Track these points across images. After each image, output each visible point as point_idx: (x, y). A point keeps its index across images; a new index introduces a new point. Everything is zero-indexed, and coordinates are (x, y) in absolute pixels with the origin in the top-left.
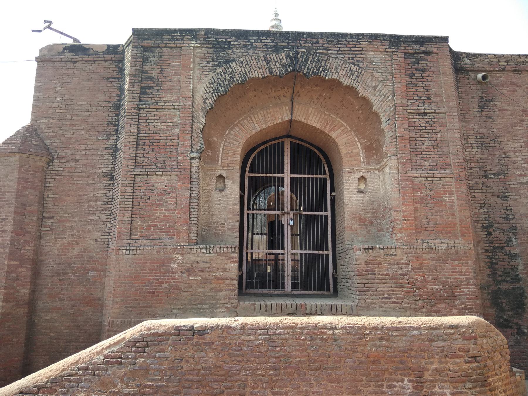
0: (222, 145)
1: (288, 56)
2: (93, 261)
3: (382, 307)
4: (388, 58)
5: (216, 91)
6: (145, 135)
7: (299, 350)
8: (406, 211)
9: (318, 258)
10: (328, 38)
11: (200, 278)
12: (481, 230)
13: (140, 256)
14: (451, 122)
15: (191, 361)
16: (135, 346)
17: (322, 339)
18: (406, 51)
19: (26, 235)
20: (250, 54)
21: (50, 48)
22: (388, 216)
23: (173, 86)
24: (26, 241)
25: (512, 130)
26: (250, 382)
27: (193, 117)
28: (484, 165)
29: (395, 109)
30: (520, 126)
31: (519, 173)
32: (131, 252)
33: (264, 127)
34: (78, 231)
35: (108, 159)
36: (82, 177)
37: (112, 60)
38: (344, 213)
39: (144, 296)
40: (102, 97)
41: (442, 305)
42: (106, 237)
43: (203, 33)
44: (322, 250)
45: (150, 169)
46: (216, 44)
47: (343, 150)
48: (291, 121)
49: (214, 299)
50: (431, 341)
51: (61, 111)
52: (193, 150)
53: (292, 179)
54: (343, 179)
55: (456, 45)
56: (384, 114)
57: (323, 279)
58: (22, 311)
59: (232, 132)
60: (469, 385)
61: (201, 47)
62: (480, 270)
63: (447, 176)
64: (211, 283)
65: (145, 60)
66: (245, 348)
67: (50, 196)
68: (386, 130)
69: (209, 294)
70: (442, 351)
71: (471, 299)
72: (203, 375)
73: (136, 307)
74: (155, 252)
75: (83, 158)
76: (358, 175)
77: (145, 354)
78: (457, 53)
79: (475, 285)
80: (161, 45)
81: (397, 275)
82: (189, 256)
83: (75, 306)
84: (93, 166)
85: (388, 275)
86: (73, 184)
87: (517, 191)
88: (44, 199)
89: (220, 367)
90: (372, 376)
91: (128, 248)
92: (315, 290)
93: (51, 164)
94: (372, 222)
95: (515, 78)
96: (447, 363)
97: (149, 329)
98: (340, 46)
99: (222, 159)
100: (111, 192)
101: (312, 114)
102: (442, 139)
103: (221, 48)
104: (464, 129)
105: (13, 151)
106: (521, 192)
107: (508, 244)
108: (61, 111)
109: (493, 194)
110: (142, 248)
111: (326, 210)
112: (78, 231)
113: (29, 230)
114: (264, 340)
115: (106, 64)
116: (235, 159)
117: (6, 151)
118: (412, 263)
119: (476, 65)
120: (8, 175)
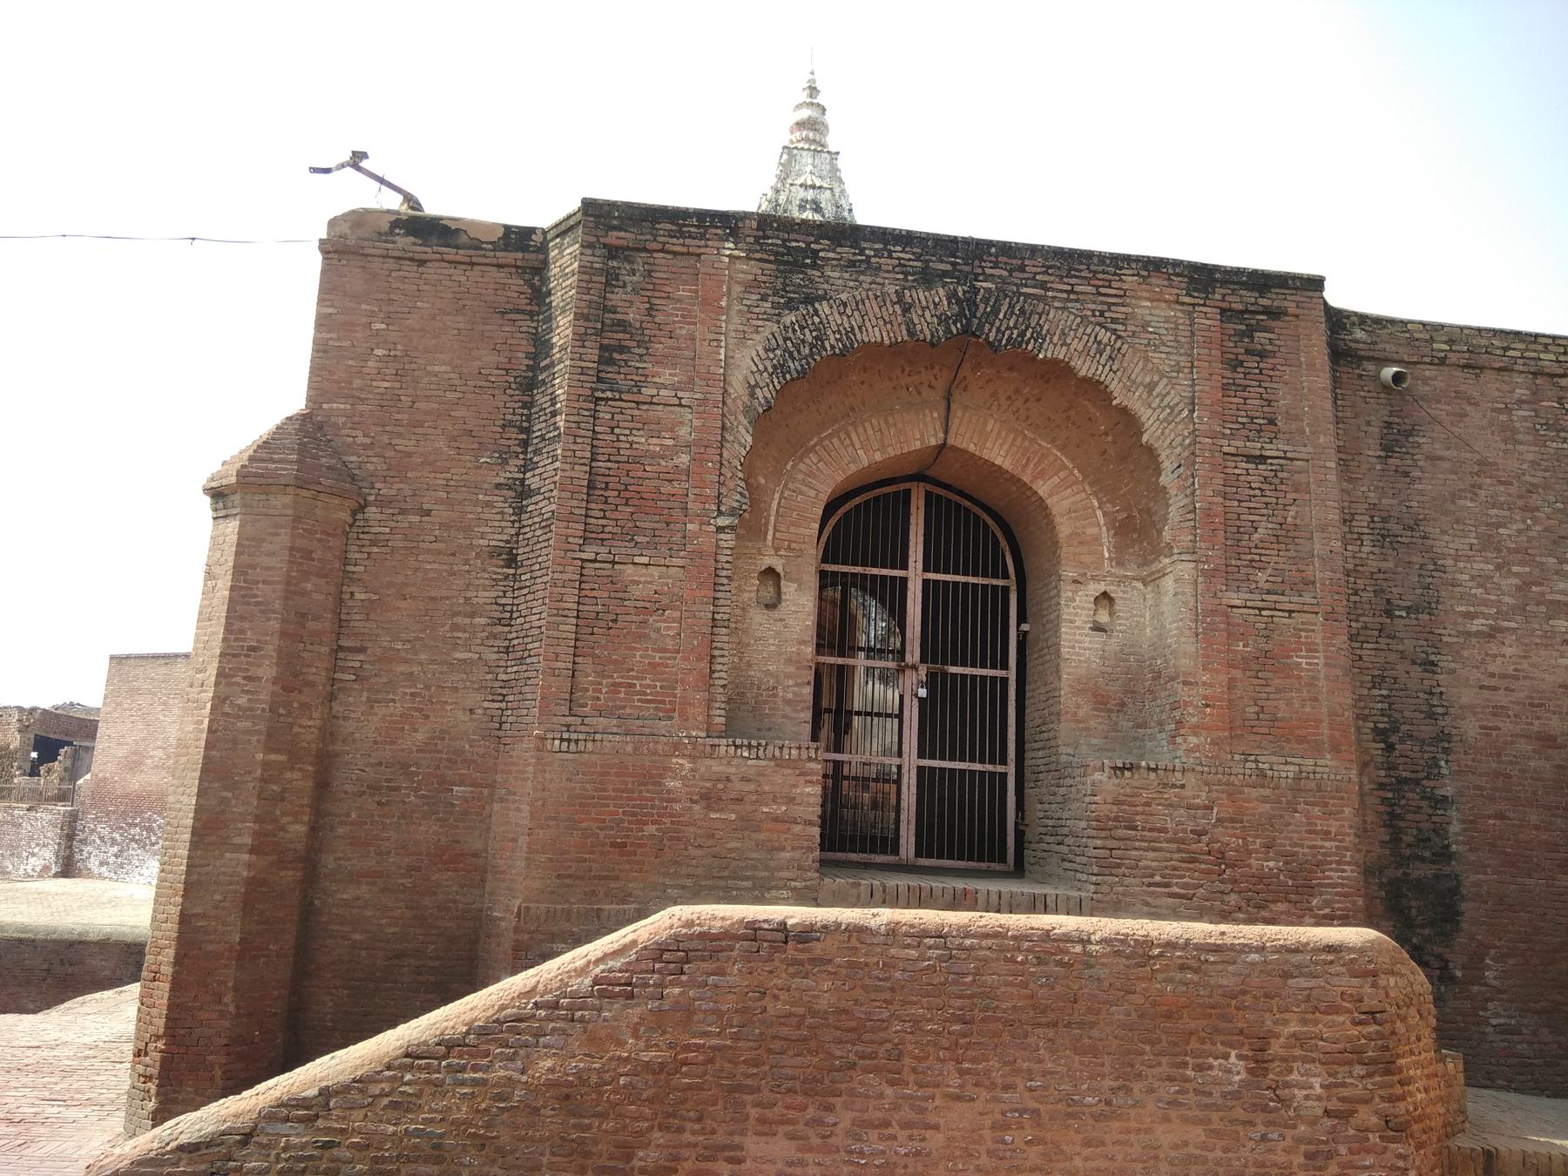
0: (777, 495)
1: (952, 296)
2: (465, 761)
3: (1147, 904)
4: (1182, 319)
5: (780, 368)
6: (609, 465)
7: (1011, 984)
8: (1211, 685)
9: (942, 779)
10: (1046, 259)
11: (733, 817)
12: (1370, 737)
13: (594, 758)
14: (1320, 483)
15: (783, 995)
16: (659, 959)
17: (1060, 963)
18: (1225, 305)
19: (306, 690)
20: (866, 286)
21: (358, 218)
22: (1164, 694)
23: (679, 349)
24: (304, 706)
25: (1453, 508)
26: (910, 1048)
27: (723, 427)
28: (1385, 585)
29: (1194, 443)
30: (1472, 500)
31: (1463, 609)
32: (573, 747)
33: (878, 457)
34: (428, 687)
35: (502, 513)
36: (439, 553)
37: (517, 267)
38: (1060, 678)
39: (602, 853)
40: (490, 358)
41: (1281, 907)
42: (497, 705)
43: (754, 224)
44: (993, 762)
45: (621, 549)
46: (783, 255)
47: (1064, 528)
48: (943, 446)
49: (766, 868)
50: (1286, 975)
51: (387, 385)
52: (723, 508)
53: (926, 582)
54: (1058, 595)
55: (1336, 296)
56: (1168, 451)
57: (992, 836)
58: (290, 876)
59: (801, 466)
60: (1359, 1070)
61: (748, 258)
62: (1365, 831)
63: (1306, 608)
64: (758, 830)
65: (612, 280)
66: (898, 975)
67: (357, 596)
68: (1173, 492)
69: (754, 855)
70: (1308, 999)
71: (1345, 895)
72: (810, 1027)
73: (582, 878)
74: (629, 748)
75: (442, 507)
76: (1095, 589)
77: (684, 978)
78: (1339, 312)
79: (1356, 864)
80: (650, 246)
81: (1185, 831)
82: (708, 762)
83: (418, 869)
84: (467, 529)
85: (1165, 830)
86: (417, 570)
87: (1457, 652)
88: (340, 602)
89: (845, 1011)
90: (1164, 1044)
91: (565, 736)
92: (970, 859)
93: (359, 516)
94: (1123, 704)
95: (1465, 382)
96: (1316, 1023)
97: (689, 924)
98: (1073, 281)
99: (776, 530)
100: (509, 594)
101: (993, 435)
102: (1298, 521)
103: (795, 263)
104: (1346, 497)
105: (283, 481)
106: (1466, 653)
107: (1429, 773)
108: (387, 385)
109: (1403, 655)
110: (598, 737)
111: (1005, 666)
112: (428, 687)
113: (311, 678)
114: (939, 958)
115: (500, 275)
116: (807, 532)
117: (262, 481)
118: (1220, 805)
119: (1380, 346)
120: (263, 540)
